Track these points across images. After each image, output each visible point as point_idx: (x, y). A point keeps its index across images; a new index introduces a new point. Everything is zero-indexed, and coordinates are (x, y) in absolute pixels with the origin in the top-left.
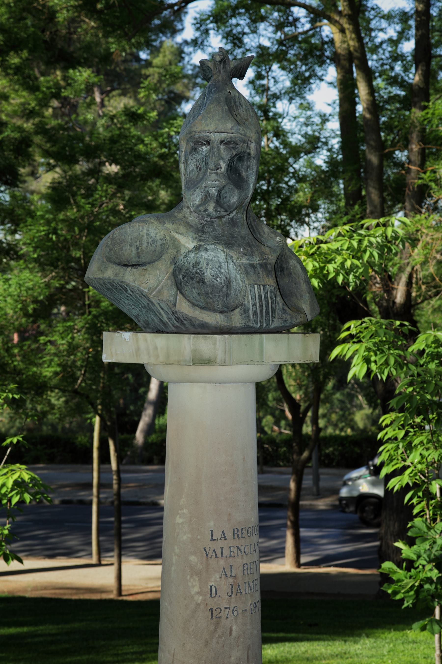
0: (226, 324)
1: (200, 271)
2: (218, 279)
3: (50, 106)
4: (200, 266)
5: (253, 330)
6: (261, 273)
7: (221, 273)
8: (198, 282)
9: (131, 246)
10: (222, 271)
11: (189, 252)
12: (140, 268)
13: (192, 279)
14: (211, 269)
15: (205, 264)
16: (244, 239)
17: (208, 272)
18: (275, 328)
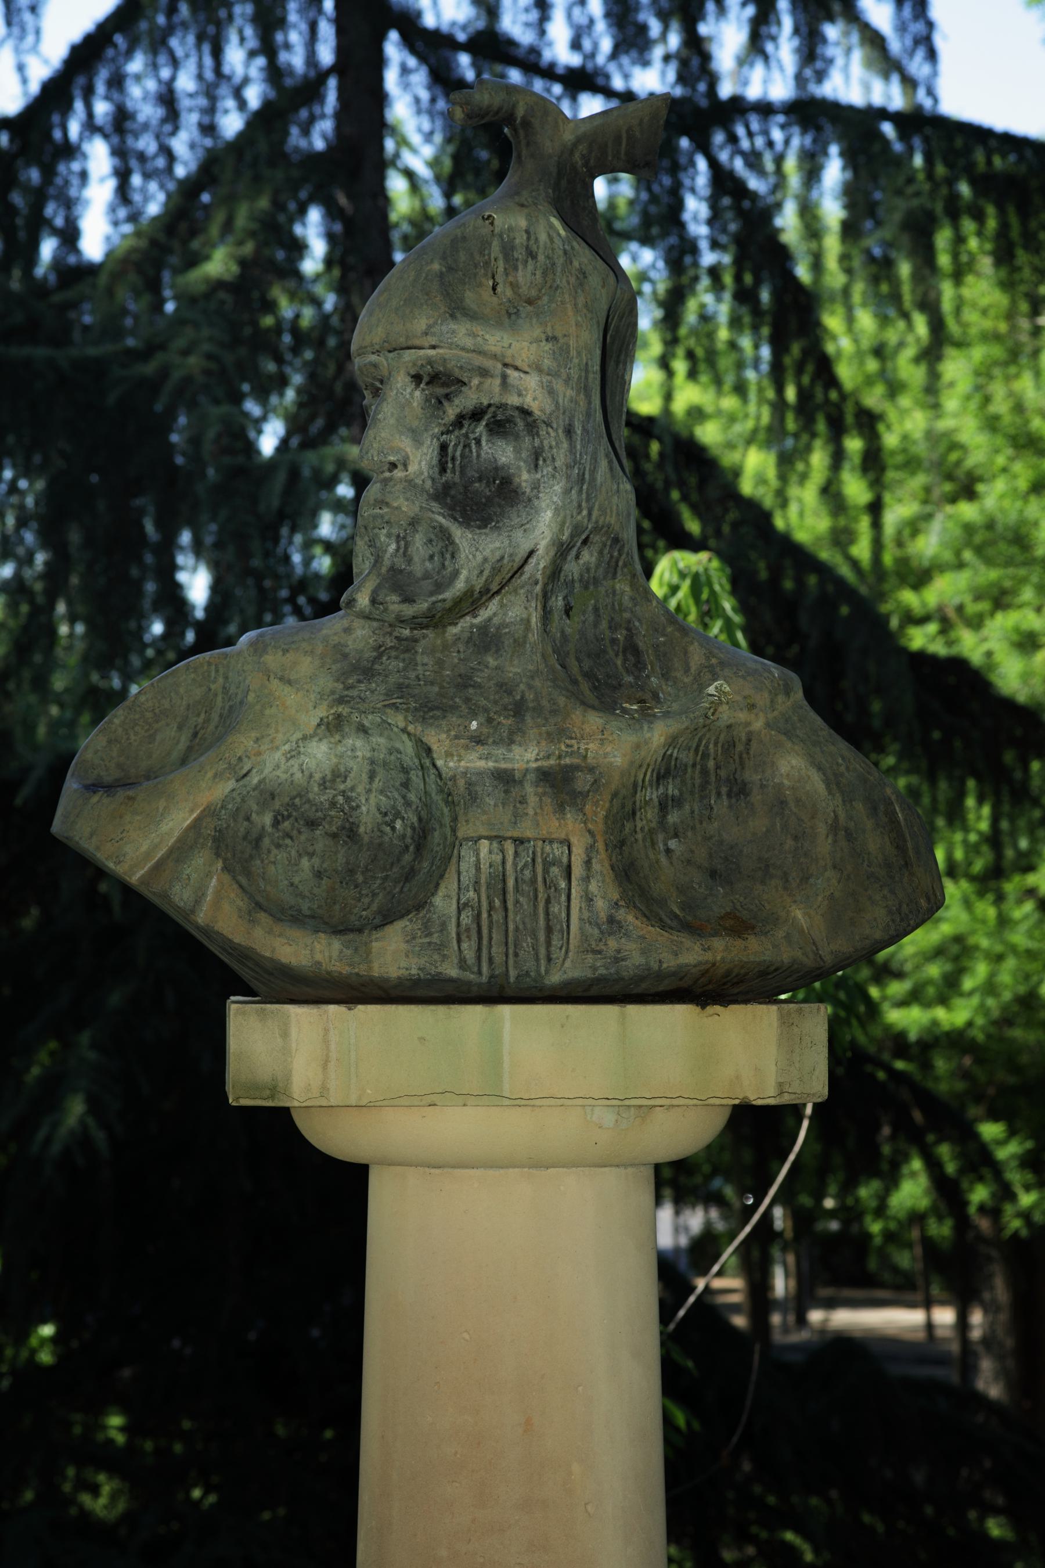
0: (346, 970)
1: (348, 799)
2: (398, 824)
3: (717, 406)
4: (349, 783)
6: (533, 800)
7: (408, 804)
8: (334, 836)
9: (180, 728)
10: (412, 797)
12: (121, 794)
14: (382, 792)
15: (365, 777)
16: (509, 692)
17: (373, 801)
18: (567, 984)
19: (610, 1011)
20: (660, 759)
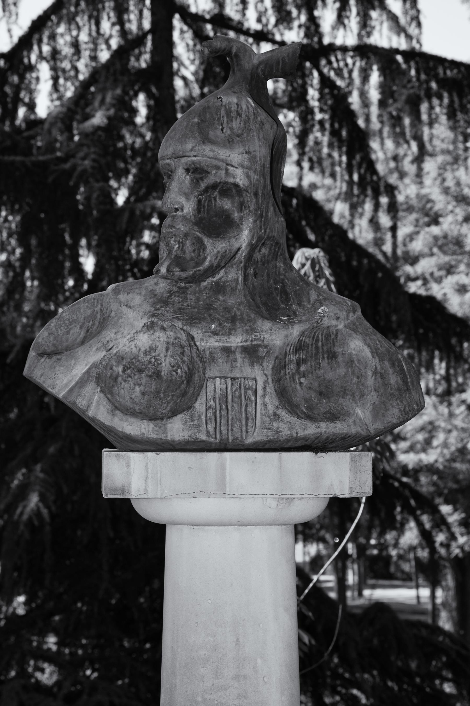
0: (155, 437)
1: (157, 360)
2: (179, 371)
4: (157, 353)
5: (202, 446)
6: (240, 360)
7: (183, 362)
8: (150, 376)
9: (81, 328)
10: (185, 359)
11: (137, 332)
12: (54, 358)
13: (140, 371)
14: (172, 357)
18: (255, 443)
19: (275, 455)
20: (297, 342)
